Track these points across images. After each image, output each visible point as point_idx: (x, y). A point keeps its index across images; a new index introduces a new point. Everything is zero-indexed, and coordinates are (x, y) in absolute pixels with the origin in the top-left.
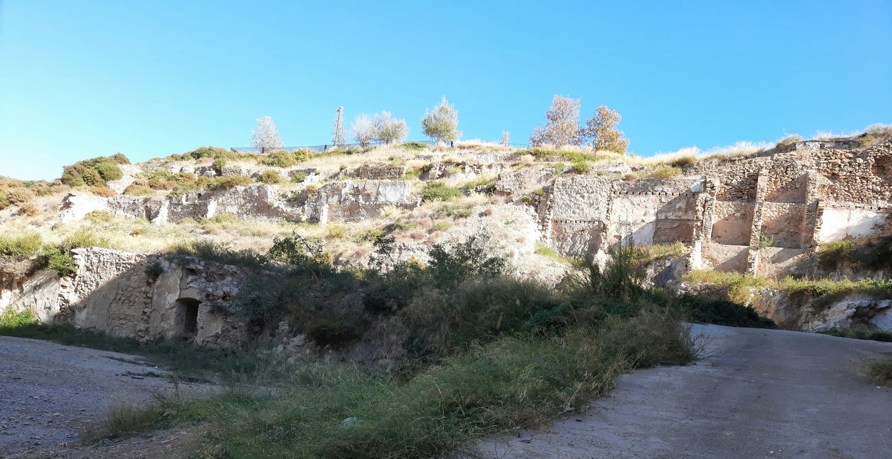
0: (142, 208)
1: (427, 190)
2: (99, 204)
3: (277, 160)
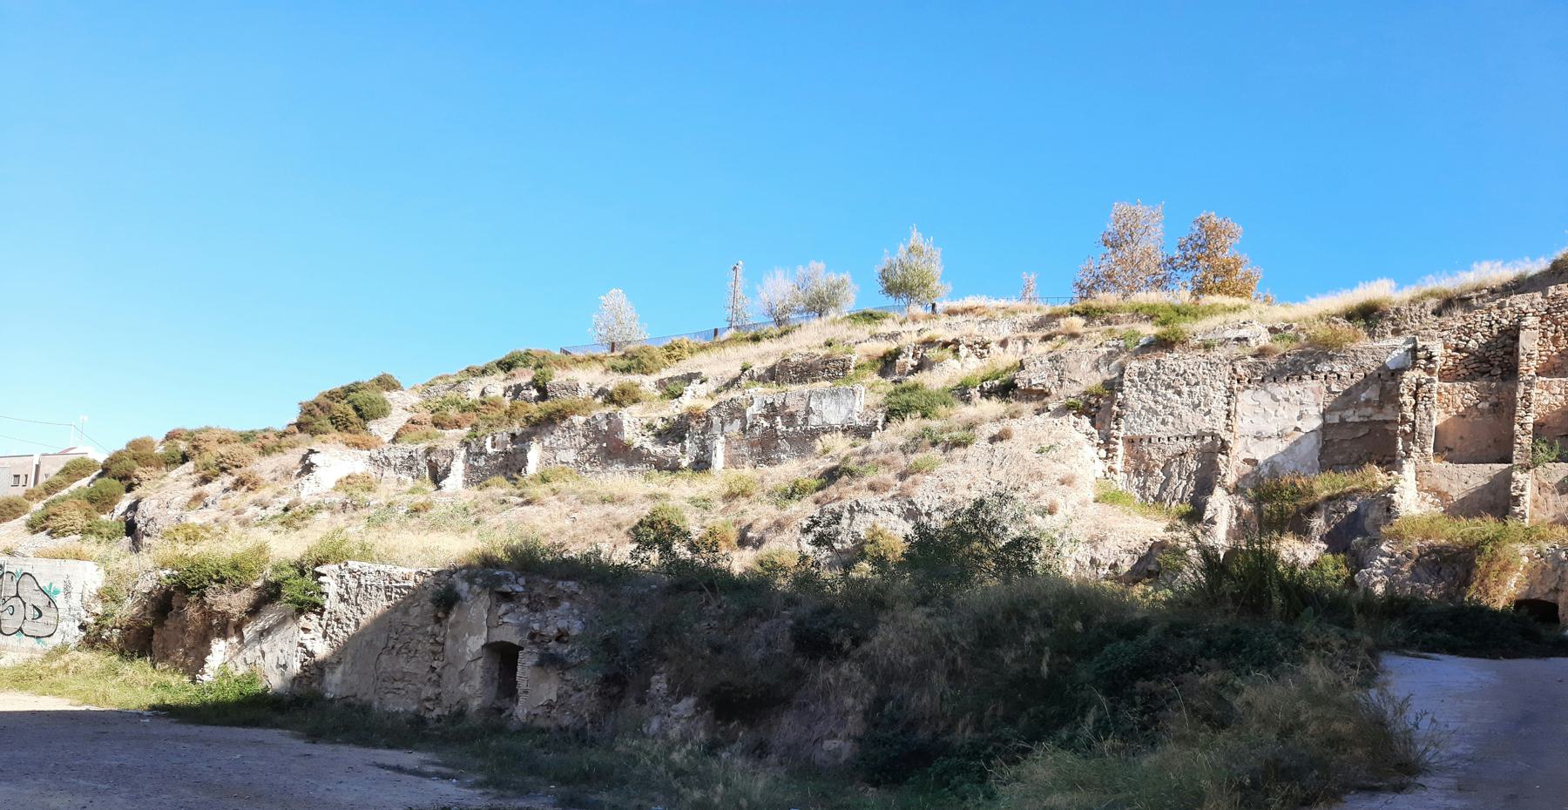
0: (423, 464)
1: (893, 399)
2: (354, 463)
3: (635, 362)
